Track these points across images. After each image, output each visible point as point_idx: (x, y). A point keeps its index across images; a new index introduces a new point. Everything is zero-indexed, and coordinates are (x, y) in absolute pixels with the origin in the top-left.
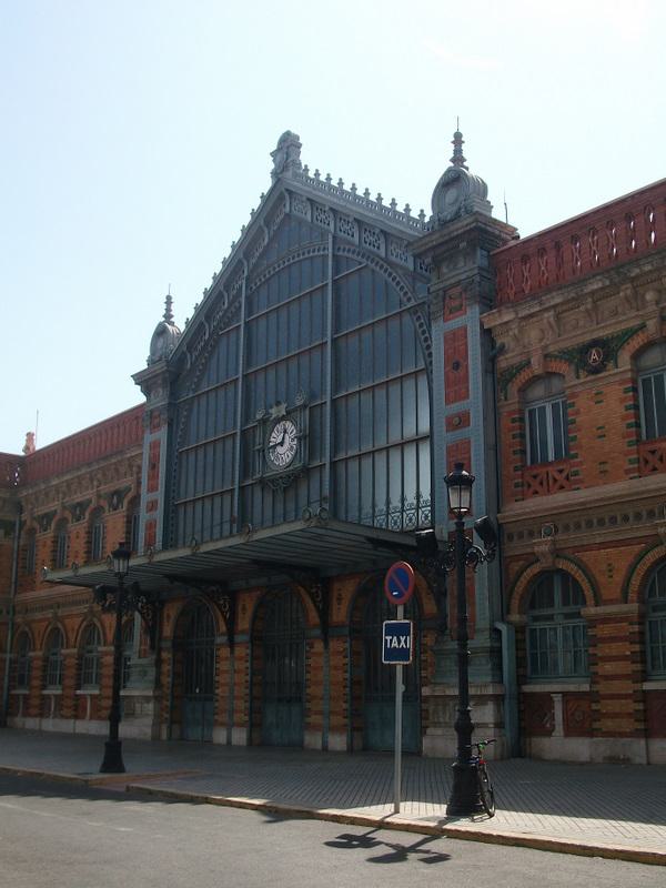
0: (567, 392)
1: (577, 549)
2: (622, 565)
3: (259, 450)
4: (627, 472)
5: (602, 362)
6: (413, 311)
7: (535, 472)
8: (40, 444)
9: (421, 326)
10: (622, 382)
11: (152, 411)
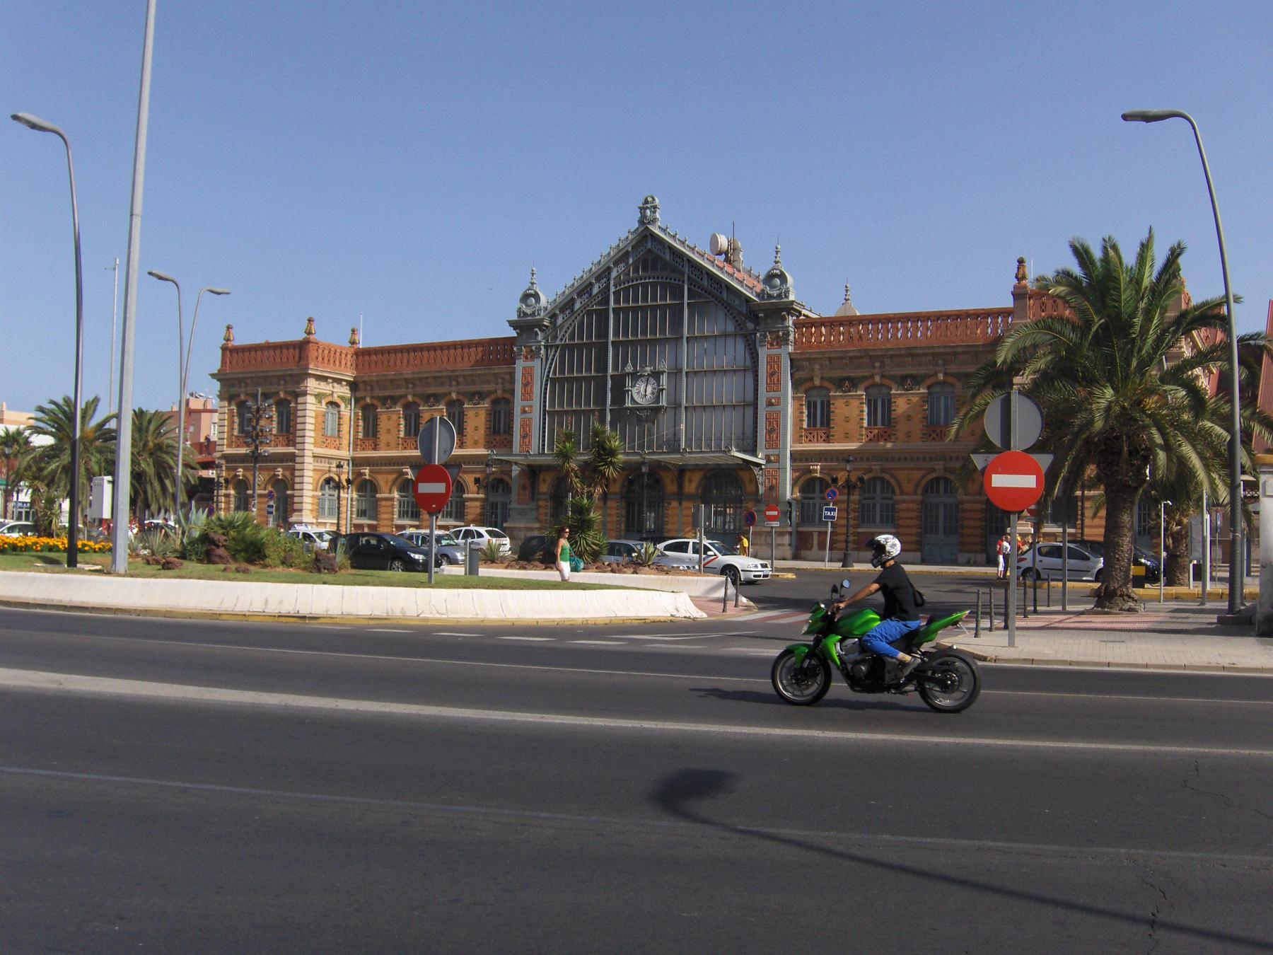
1: (893, 469)
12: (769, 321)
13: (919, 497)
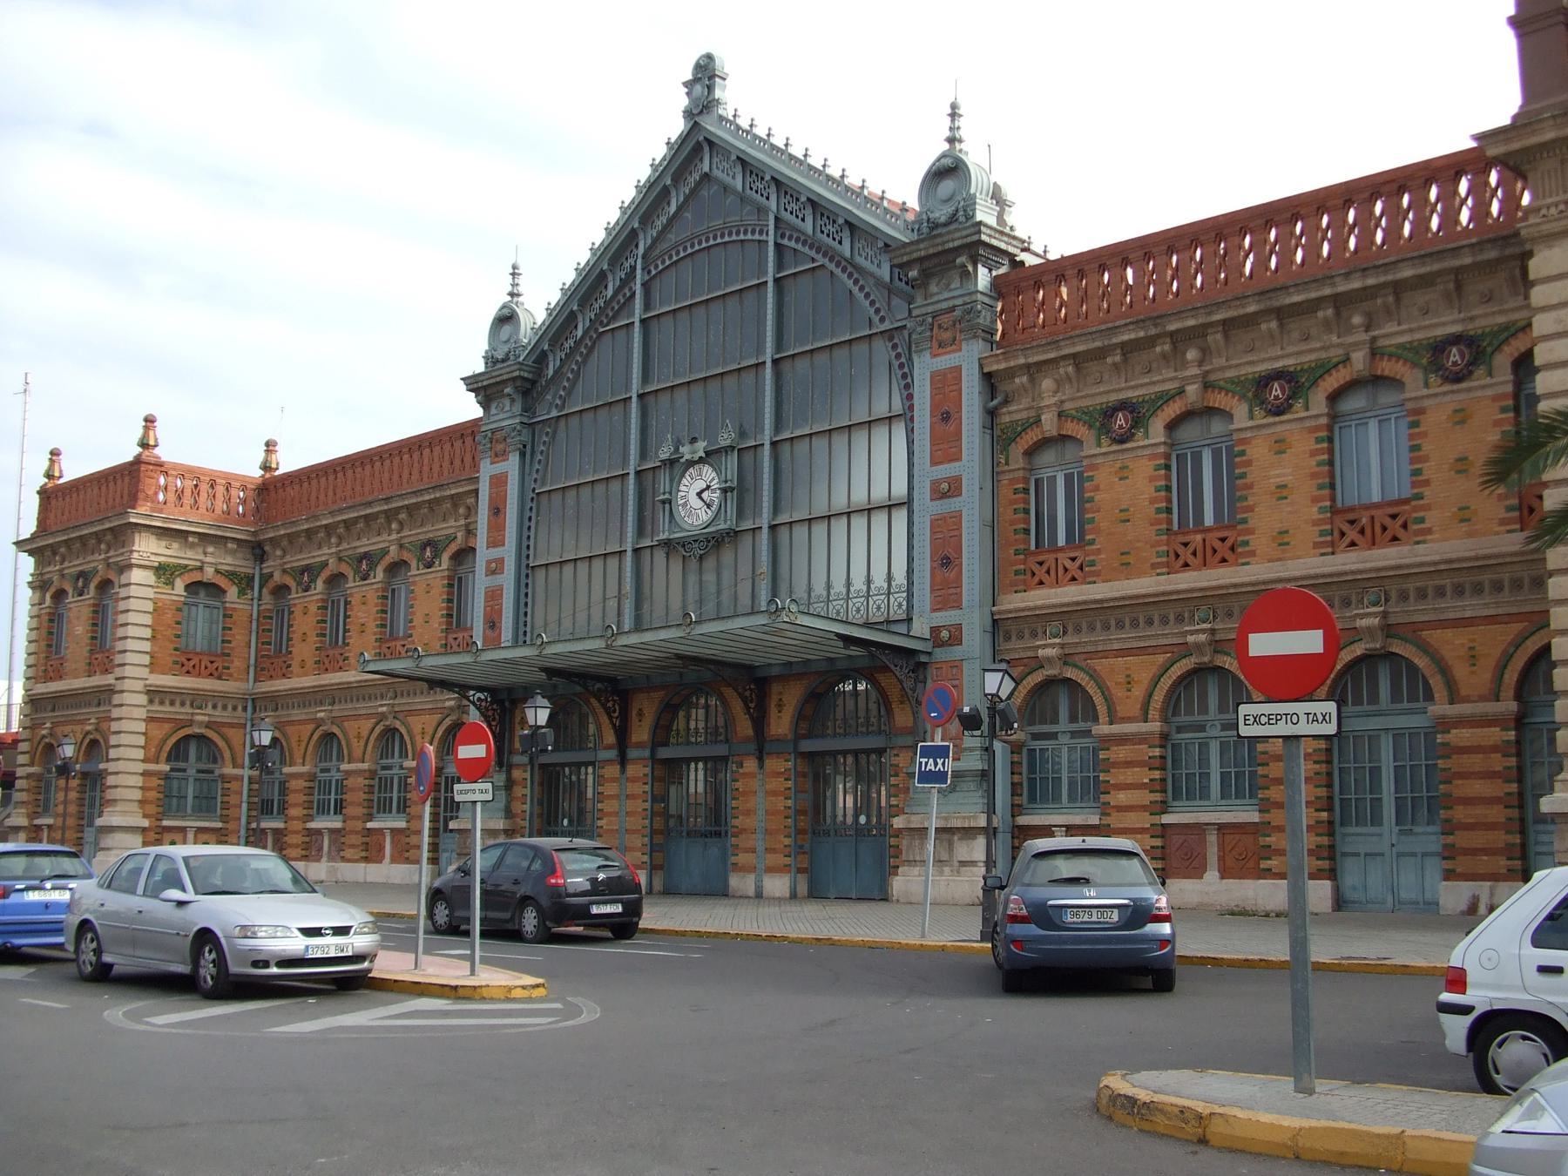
0: (1235, 437)
2: (1143, 677)
3: (663, 502)
4: (1154, 566)
5: (1130, 429)
6: (889, 334)
7: (1041, 558)
8: (288, 463)
9: (898, 356)
10: (1153, 457)
11: (493, 431)
12: (933, 288)
13: (1155, 726)
